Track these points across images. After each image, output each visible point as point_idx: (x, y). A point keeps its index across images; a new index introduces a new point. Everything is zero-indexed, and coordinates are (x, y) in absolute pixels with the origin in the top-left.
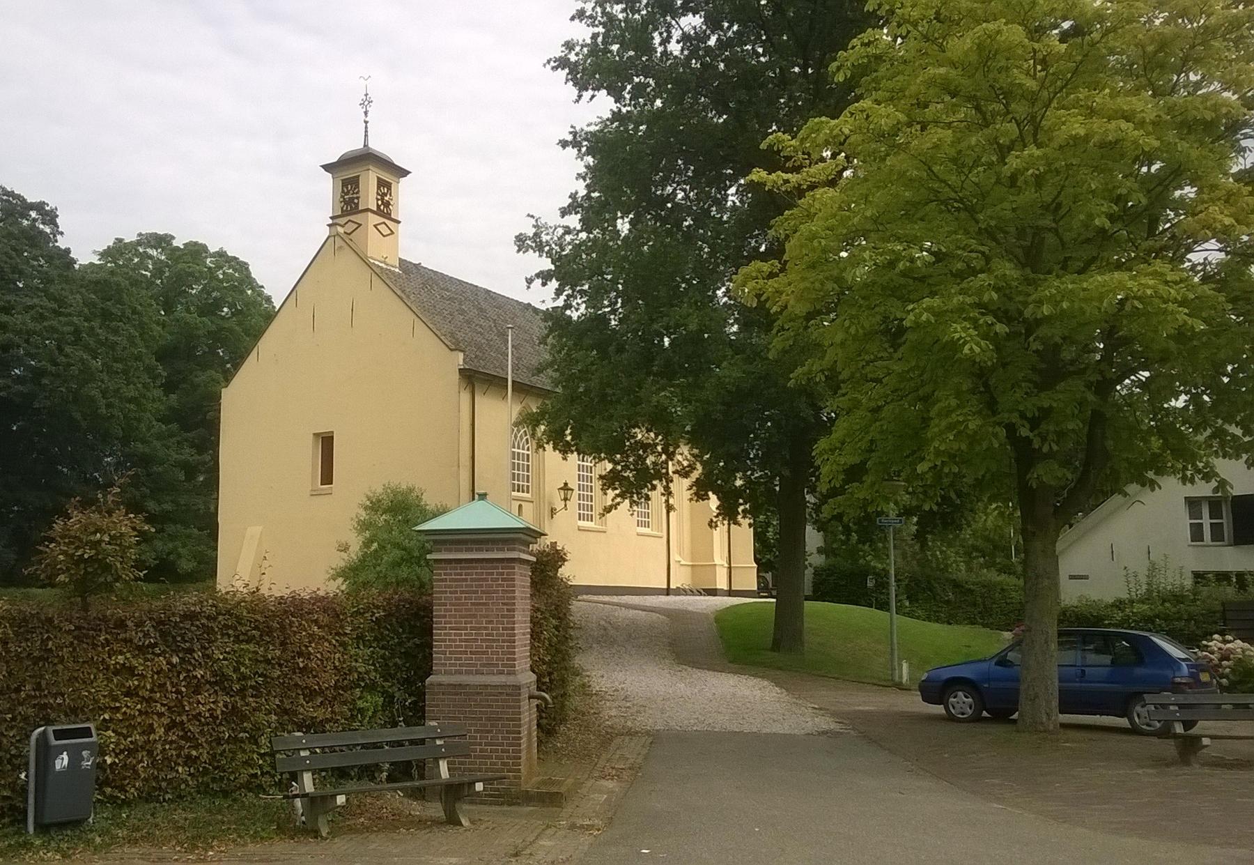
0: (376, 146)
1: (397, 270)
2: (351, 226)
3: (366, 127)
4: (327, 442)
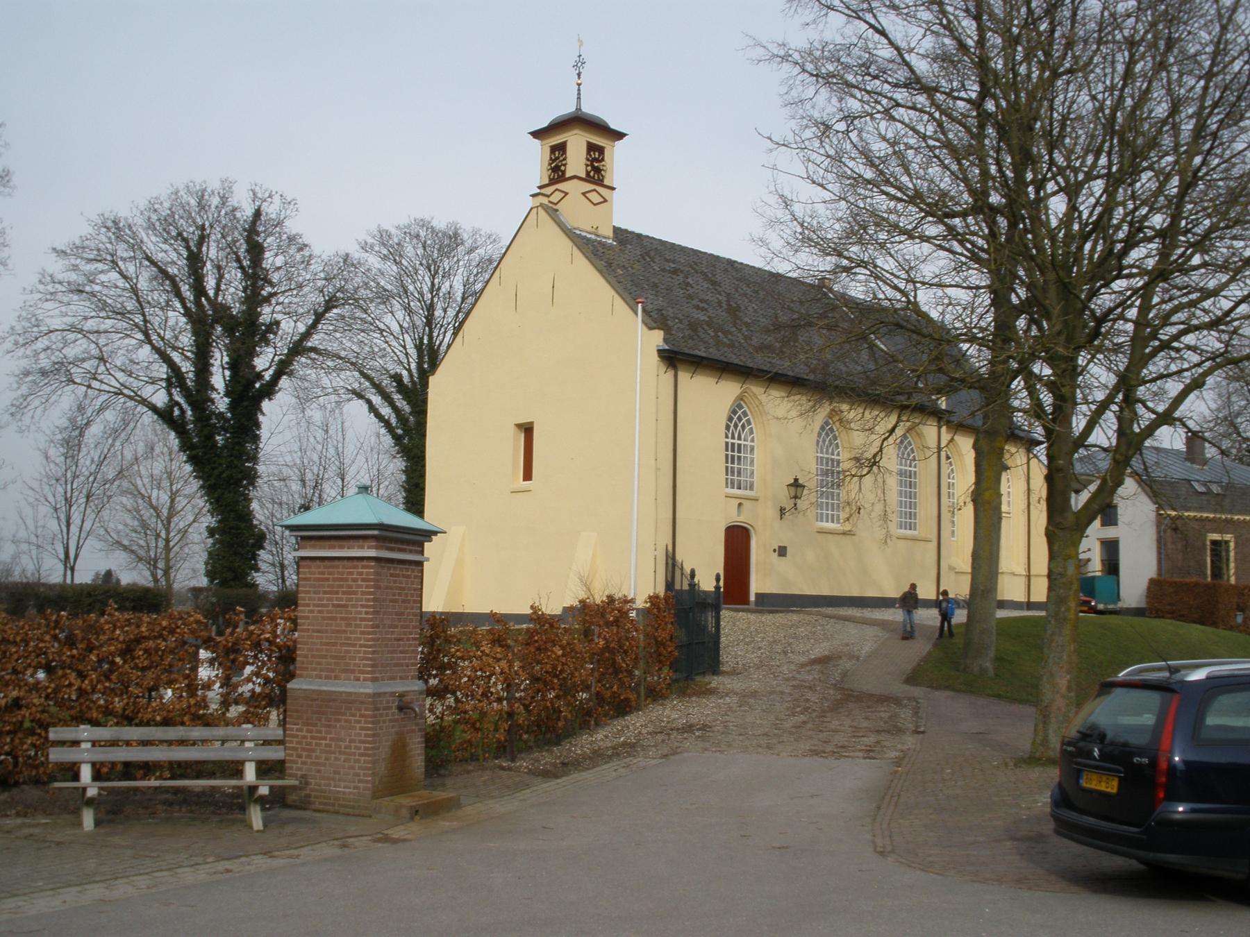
0: (589, 109)
1: (610, 241)
2: (558, 196)
3: (579, 90)
4: (527, 430)
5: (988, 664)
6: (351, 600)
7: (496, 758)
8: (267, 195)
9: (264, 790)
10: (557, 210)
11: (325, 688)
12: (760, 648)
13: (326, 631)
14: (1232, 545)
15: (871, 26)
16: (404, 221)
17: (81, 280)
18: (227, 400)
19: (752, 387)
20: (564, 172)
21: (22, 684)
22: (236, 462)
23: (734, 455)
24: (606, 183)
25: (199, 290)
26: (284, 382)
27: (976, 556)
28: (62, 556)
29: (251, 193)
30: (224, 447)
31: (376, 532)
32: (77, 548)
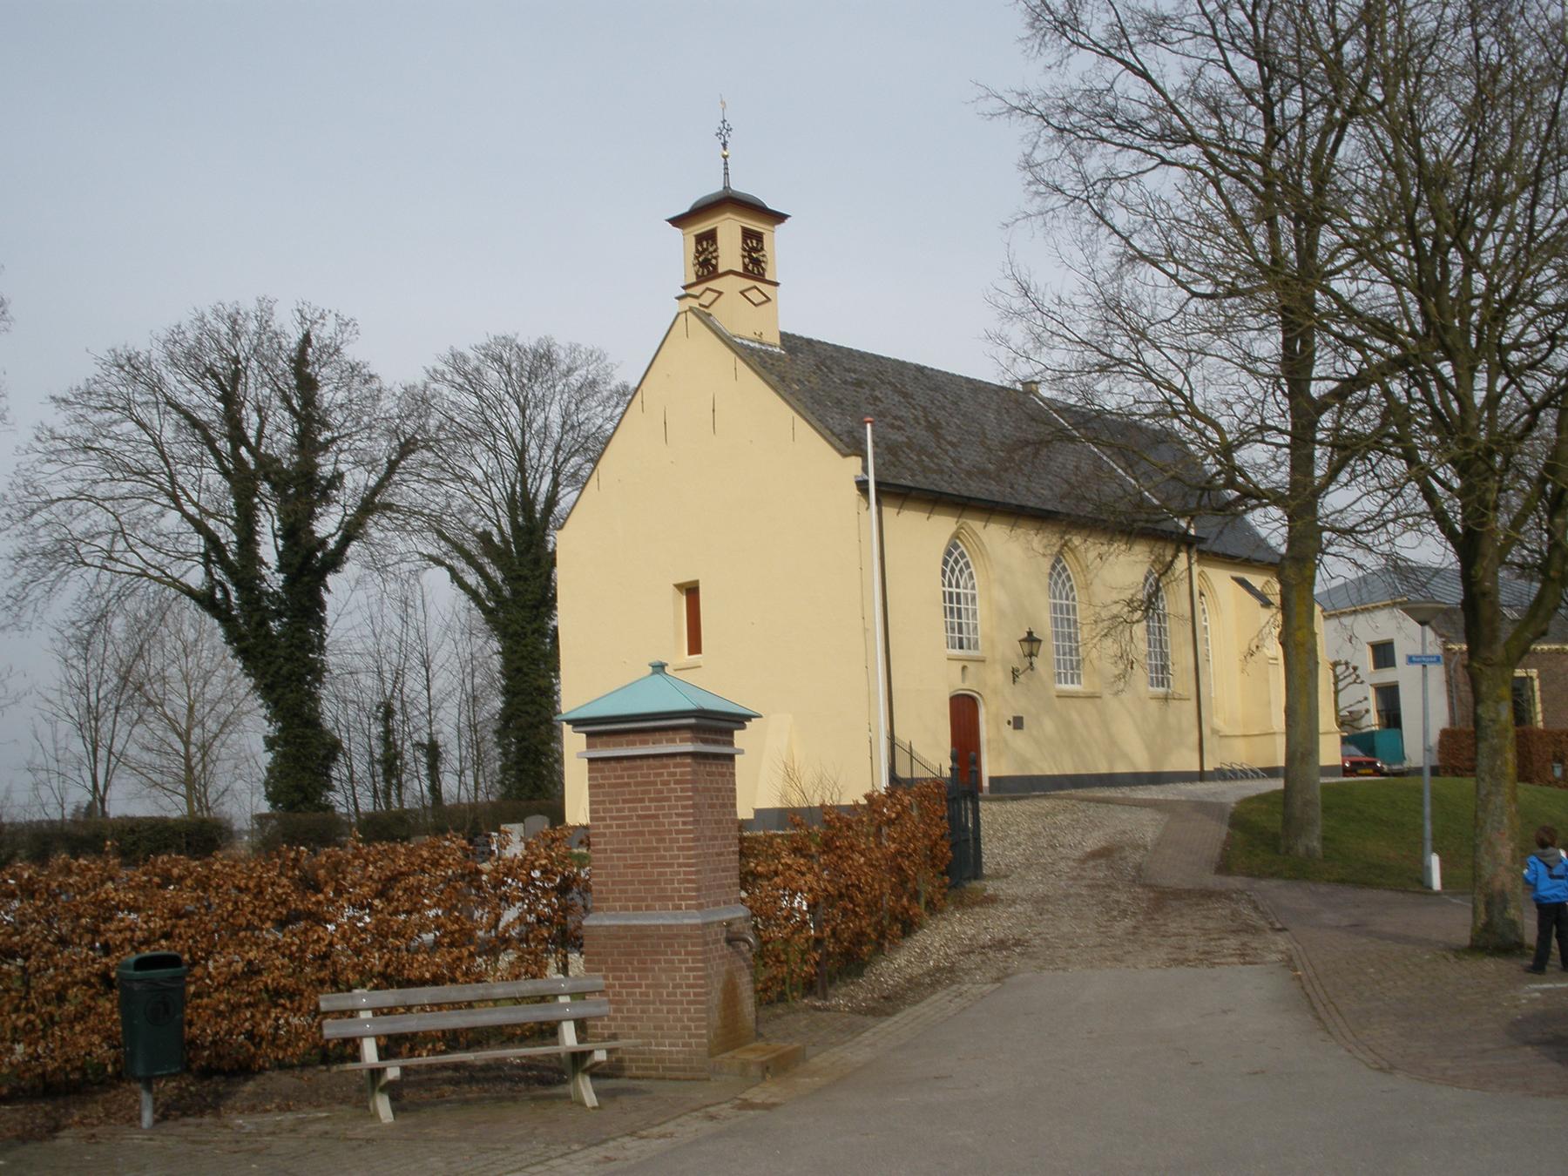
0: (740, 186)
1: (777, 350)
2: (709, 296)
3: (726, 163)
4: (691, 592)
5: (1315, 844)
6: (663, 808)
7: (804, 996)
8: (317, 315)
9: (393, 1073)
10: (710, 315)
11: (635, 922)
12: (1019, 844)
13: (631, 850)
14: (1536, 684)
15: (1128, 65)
16: (482, 340)
17: (87, 434)
18: (281, 576)
19: (970, 522)
20: (715, 267)
21: (260, 941)
22: (298, 654)
23: (954, 605)
24: (768, 277)
25: (237, 436)
26: (354, 548)
27: (1290, 712)
28: (90, 784)
29: (298, 314)
30: (281, 635)
31: (692, 721)
32: (107, 773)
